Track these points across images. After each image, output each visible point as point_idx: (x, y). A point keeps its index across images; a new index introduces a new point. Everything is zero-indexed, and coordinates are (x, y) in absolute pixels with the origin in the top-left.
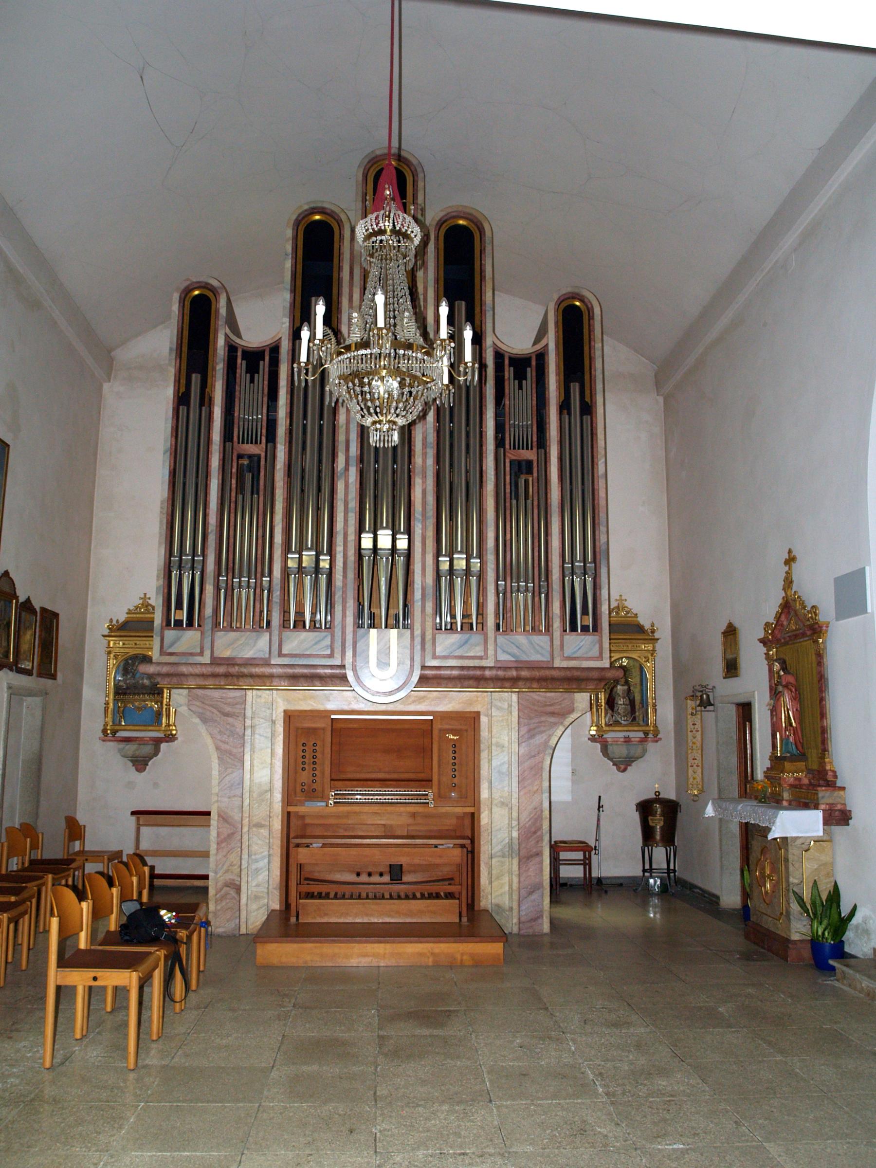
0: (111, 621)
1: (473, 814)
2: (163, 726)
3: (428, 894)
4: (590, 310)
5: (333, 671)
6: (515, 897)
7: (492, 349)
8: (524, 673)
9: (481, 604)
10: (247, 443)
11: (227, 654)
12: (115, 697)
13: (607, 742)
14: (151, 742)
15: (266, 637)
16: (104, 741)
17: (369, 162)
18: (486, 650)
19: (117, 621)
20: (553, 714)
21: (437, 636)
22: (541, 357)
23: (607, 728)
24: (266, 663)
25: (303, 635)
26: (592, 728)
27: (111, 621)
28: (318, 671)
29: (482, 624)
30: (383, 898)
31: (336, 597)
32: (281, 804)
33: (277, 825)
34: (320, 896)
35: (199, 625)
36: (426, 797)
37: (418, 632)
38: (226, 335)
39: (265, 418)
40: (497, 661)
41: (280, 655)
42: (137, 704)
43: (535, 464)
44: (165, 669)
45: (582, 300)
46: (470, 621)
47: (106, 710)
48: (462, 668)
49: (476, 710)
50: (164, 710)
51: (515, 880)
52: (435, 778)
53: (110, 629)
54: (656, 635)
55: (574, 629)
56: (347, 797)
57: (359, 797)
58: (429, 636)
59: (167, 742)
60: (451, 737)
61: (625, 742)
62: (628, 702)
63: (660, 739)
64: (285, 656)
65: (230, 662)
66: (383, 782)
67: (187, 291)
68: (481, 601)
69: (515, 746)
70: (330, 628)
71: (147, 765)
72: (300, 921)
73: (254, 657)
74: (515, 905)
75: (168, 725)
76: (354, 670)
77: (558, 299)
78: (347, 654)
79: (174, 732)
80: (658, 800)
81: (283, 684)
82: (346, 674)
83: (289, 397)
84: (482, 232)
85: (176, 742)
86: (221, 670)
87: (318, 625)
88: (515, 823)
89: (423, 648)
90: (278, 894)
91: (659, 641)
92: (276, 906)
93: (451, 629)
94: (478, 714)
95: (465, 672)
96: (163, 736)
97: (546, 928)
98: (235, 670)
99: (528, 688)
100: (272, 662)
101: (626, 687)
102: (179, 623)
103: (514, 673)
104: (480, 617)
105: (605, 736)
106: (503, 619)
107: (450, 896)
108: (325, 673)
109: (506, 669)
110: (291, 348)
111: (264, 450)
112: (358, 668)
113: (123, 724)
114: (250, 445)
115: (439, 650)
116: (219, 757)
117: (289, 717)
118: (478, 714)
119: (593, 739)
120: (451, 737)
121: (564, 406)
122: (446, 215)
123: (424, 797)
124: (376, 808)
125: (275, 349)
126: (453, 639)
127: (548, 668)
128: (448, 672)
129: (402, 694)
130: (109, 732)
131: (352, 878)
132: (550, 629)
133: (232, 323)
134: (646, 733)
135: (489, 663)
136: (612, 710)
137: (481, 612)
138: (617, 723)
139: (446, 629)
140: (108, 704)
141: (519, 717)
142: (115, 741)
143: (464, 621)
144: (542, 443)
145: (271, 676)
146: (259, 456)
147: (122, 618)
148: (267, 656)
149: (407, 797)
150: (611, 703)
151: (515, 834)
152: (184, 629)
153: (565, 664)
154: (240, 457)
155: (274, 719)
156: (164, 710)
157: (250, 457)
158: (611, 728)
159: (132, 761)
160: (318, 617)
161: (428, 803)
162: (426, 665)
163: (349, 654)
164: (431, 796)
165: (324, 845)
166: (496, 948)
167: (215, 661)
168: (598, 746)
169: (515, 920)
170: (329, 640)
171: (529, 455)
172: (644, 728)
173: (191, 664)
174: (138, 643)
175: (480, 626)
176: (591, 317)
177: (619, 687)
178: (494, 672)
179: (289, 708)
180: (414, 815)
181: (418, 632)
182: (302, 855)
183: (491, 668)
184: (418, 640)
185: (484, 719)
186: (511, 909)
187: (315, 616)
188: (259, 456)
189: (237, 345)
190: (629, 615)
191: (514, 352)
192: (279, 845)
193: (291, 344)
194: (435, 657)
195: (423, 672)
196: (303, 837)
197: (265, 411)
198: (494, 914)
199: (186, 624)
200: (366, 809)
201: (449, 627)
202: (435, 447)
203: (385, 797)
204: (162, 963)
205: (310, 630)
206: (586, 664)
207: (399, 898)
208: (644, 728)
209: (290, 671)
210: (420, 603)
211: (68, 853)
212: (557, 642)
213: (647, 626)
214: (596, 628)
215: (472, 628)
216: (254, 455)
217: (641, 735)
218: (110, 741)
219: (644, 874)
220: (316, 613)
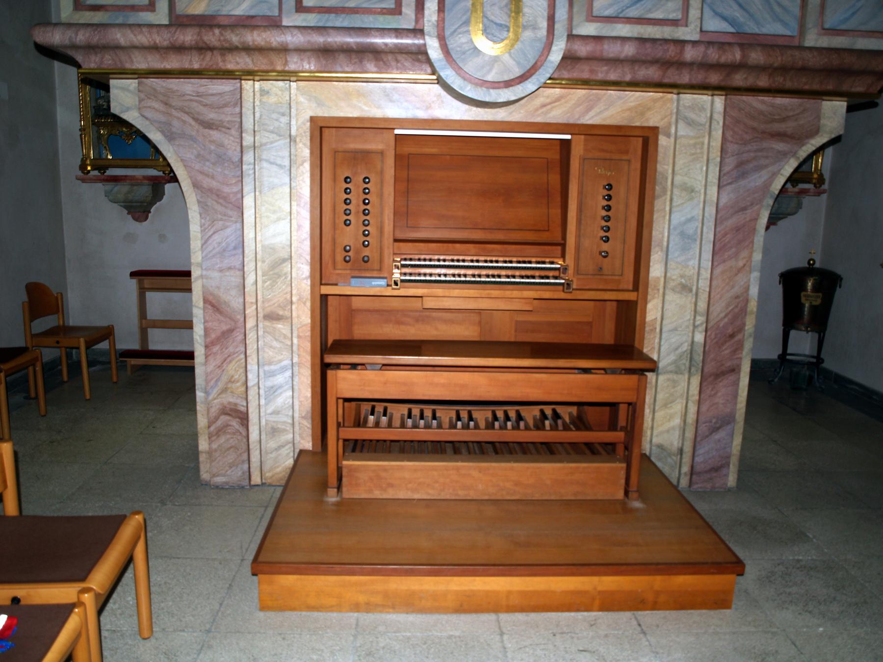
6: (690, 434)
49: (651, 124)
51: (693, 409)
69: (713, 191)
74: (688, 448)
88: (700, 319)
90: (309, 426)
92: (308, 445)
94: (655, 130)
97: (732, 480)
109: (722, 46)
148: (276, 13)
151: (699, 337)
153: (825, 42)
155: (293, 133)
159: (126, 207)
185: (663, 141)
194: (592, 18)
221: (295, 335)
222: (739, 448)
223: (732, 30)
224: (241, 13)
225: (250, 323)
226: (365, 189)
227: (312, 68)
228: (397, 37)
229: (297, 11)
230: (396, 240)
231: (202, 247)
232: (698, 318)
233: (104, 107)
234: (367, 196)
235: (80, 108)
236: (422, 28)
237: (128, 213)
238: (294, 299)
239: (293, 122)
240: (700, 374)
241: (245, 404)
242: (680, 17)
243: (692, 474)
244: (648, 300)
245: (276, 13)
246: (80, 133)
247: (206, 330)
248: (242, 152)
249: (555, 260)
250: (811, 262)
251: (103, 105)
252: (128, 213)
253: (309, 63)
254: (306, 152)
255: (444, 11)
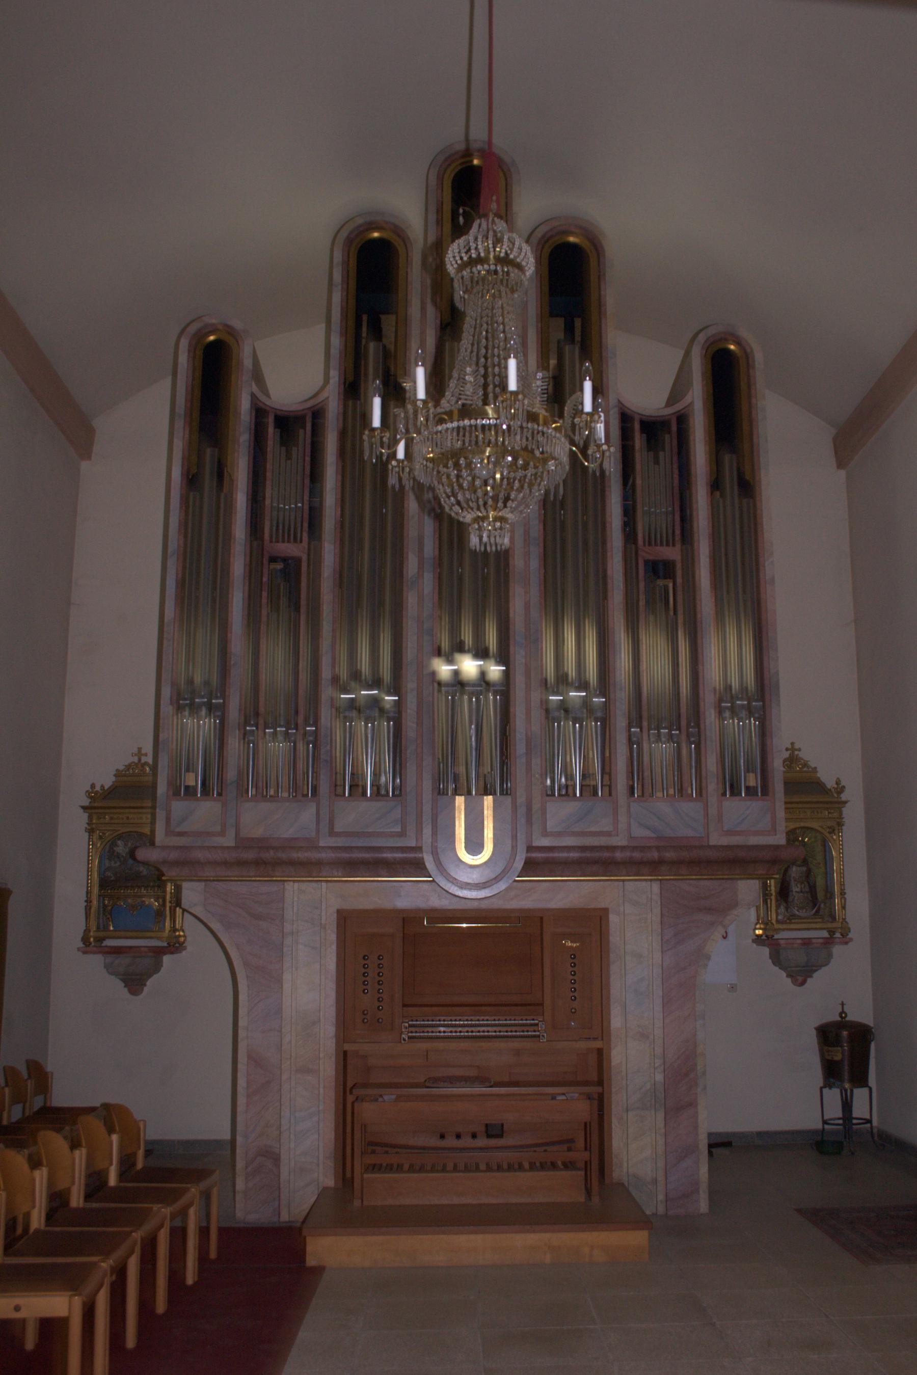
0: (93, 786)
1: (600, 1052)
2: (167, 931)
3: (541, 1163)
4: (748, 356)
5: (405, 855)
6: (661, 1164)
7: (616, 410)
8: (669, 855)
9: (607, 760)
10: (283, 542)
11: (258, 832)
12: (100, 890)
13: (779, 945)
14: (150, 954)
15: (312, 809)
16: (85, 953)
17: (446, 160)
18: (616, 822)
19: (102, 786)
20: (709, 910)
21: (548, 804)
22: (682, 419)
23: (780, 926)
24: (313, 845)
25: (363, 805)
26: (758, 926)
27: (93, 786)
28: (385, 855)
29: (609, 788)
30: (477, 1169)
31: (408, 751)
32: (334, 1041)
33: (328, 1068)
34: (390, 1168)
35: (220, 794)
36: (535, 1028)
37: (521, 799)
38: (253, 396)
39: (306, 507)
40: (631, 838)
41: (332, 833)
42: (130, 901)
43: (679, 566)
44: (173, 856)
45: (738, 343)
46: (592, 783)
47: (88, 909)
48: (583, 849)
49: (602, 905)
50: (168, 908)
51: (661, 1141)
52: (548, 1002)
53: (91, 798)
54: (844, 797)
55: (735, 791)
56: (426, 1029)
57: (442, 1029)
58: (536, 806)
59: (172, 953)
60: (569, 944)
61: (804, 944)
62: (807, 889)
63: (851, 940)
64: (338, 835)
65: (262, 844)
66: (476, 1007)
67: (200, 335)
68: (607, 754)
69: (658, 956)
70: (400, 795)
71: (145, 985)
72: (365, 1203)
73: (295, 836)
74: (661, 1178)
75: (174, 929)
76: (435, 853)
77: (706, 342)
78: (425, 831)
79: (182, 939)
80: (842, 1024)
81: (336, 874)
82: (423, 858)
83: (340, 477)
84: (598, 249)
85: (184, 953)
86: (250, 855)
87: (383, 792)
88: (658, 1062)
89: (529, 821)
90: (332, 1165)
91: (847, 805)
92: (330, 1182)
93: (567, 794)
94: (606, 911)
95: (588, 854)
96: (165, 944)
97: (703, 1206)
98: (269, 855)
99: (675, 875)
100: (322, 844)
101: (804, 869)
102: (190, 791)
103: (655, 855)
104: (606, 777)
105: (776, 937)
106: (638, 779)
107: (568, 1165)
108: (395, 859)
109: (642, 849)
110: (341, 411)
111: (306, 551)
112: (439, 850)
113: (112, 928)
114: (286, 544)
115: (550, 825)
116: (247, 977)
117: (344, 918)
118: (606, 911)
119: (758, 940)
120: (569, 944)
121: (716, 485)
122: (551, 230)
123: (532, 1028)
124: (464, 1045)
125: (317, 414)
126: (570, 808)
127: (701, 847)
128: (564, 855)
129: (502, 886)
130: (92, 939)
131: (434, 1142)
132: (704, 792)
133: (258, 376)
134: (832, 932)
135: (619, 841)
136: (786, 901)
137: (607, 770)
138: (791, 918)
139: (560, 795)
140: (91, 902)
141: (662, 915)
142: (99, 952)
143: (584, 783)
144: (687, 536)
145: (320, 863)
146: (298, 561)
147: (108, 781)
148: (313, 834)
149: (509, 1029)
150: (784, 892)
151: (659, 1077)
152: (198, 799)
153: (725, 841)
154: (273, 559)
155: (323, 922)
156: (168, 908)
157: (285, 560)
158: (785, 926)
159: (123, 980)
160: (383, 779)
161: (539, 1036)
162: (534, 845)
163: (427, 831)
164: (542, 1026)
165: (399, 1098)
166: (638, 1238)
167: (243, 843)
168: (766, 951)
169: (661, 1197)
170: (399, 811)
171: (672, 553)
172: (830, 925)
173: (208, 848)
174: (131, 816)
175: (606, 789)
176: (750, 365)
177: (794, 869)
178: (628, 854)
179: (345, 907)
180: (517, 1053)
181: (521, 799)
182: (368, 1111)
183: (623, 848)
184: (522, 811)
185: (613, 919)
186: (655, 1181)
187: (379, 780)
188: (298, 561)
189: (268, 408)
190: (805, 769)
191: (647, 413)
192: (333, 1098)
193: (341, 407)
194: (545, 833)
195: (529, 855)
196: (365, 1085)
197: (306, 497)
198: (631, 1189)
199: (202, 792)
200: (453, 1045)
201: (564, 792)
202: (542, 545)
203: (479, 1029)
204: (138, 1249)
205: (371, 799)
206: (754, 840)
207: (499, 1168)
208: (830, 925)
209: (345, 855)
210: (524, 760)
211: (24, 1106)
212: (713, 811)
213: (830, 784)
214: (765, 790)
215: (595, 793)
216: (293, 558)
217: (825, 934)
218: (94, 953)
219: (823, 1126)
220: (380, 775)
221: (322, 1086)
222: (707, 1175)
223: (653, 835)
224: (287, 837)
225: (284, 1077)
226: (379, 964)
227: (340, 874)
228: (403, 853)
229: (329, 836)
230: (404, 1005)
231: (248, 1013)
232: (656, 1061)
233: (112, 879)
234: (381, 970)
235: (88, 876)
236: (420, 845)
237: (125, 987)
238: (321, 1055)
239: (323, 914)
240: (663, 1109)
241: (278, 1146)
242: (611, 829)
243: (666, 1201)
244: (612, 1047)
245: (313, 834)
246: (86, 904)
247: (248, 1082)
248: (283, 937)
249: (535, 1018)
250: (843, 1015)
251: (111, 877)
252: (125, 987)
253: (338, 871)
254: (333, 937)
255: (437, 835)
